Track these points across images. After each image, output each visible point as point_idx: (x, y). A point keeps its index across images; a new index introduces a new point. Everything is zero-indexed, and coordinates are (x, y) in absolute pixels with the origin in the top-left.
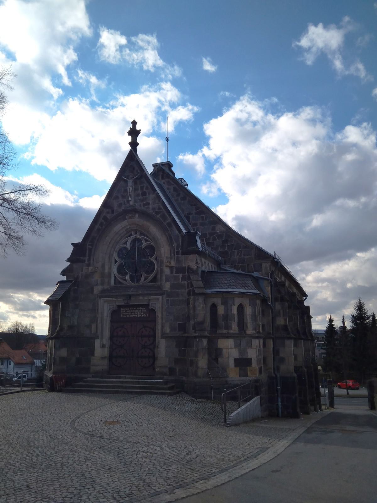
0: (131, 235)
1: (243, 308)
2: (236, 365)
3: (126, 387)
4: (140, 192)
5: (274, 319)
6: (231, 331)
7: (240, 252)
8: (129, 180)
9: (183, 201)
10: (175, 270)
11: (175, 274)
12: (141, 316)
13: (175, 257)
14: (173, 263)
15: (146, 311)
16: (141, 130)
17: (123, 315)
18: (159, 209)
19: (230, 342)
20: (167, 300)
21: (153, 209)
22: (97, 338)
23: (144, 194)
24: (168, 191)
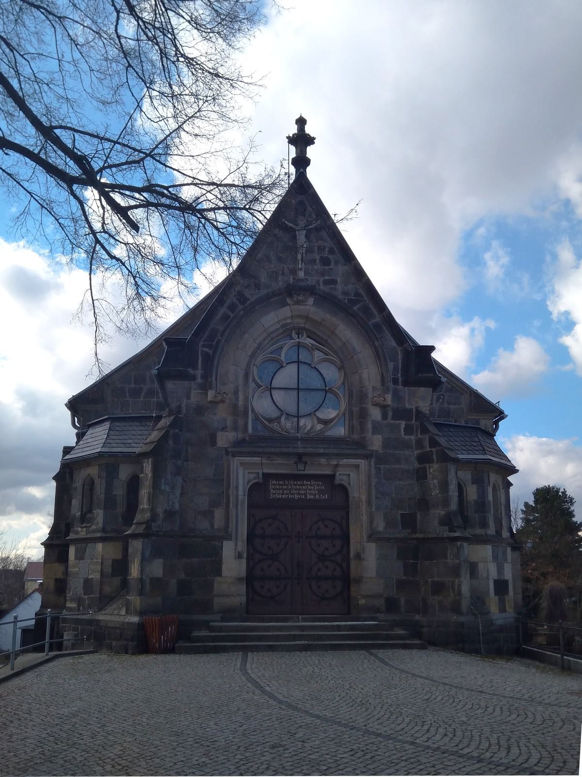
3: (320, 638)
10: (391, 414)
11: (392, 420)
12: (312, 497)
15: (323, 487)
17: (274, 494)
18: (357, 294)
19: (487, 551)
20: (378, 469)
22: (229, 538)
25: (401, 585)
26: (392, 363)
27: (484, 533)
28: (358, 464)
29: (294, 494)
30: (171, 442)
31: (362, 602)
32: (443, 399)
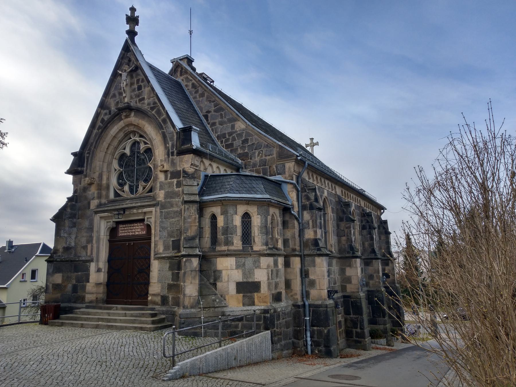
1: (250, 219)
2: (238, 292)
4: (136, 86)
5: (301, 232)
6: (232, 248)
7: (261, 152)
8: (123, 74)
9: (201, 98)
11: (170, 179)
12: (138, 233)
13: (170, 158)
14: (167, 167)
17: (121, 233)
18: (155, 103)
20: (161, 212)
21: (149, 104)
22: (92, 261)
23: (140, 88)
24: (187, 89)
25: (170, 287)
26: (171, 142)
28: (151, 210)
32: (262, 154)
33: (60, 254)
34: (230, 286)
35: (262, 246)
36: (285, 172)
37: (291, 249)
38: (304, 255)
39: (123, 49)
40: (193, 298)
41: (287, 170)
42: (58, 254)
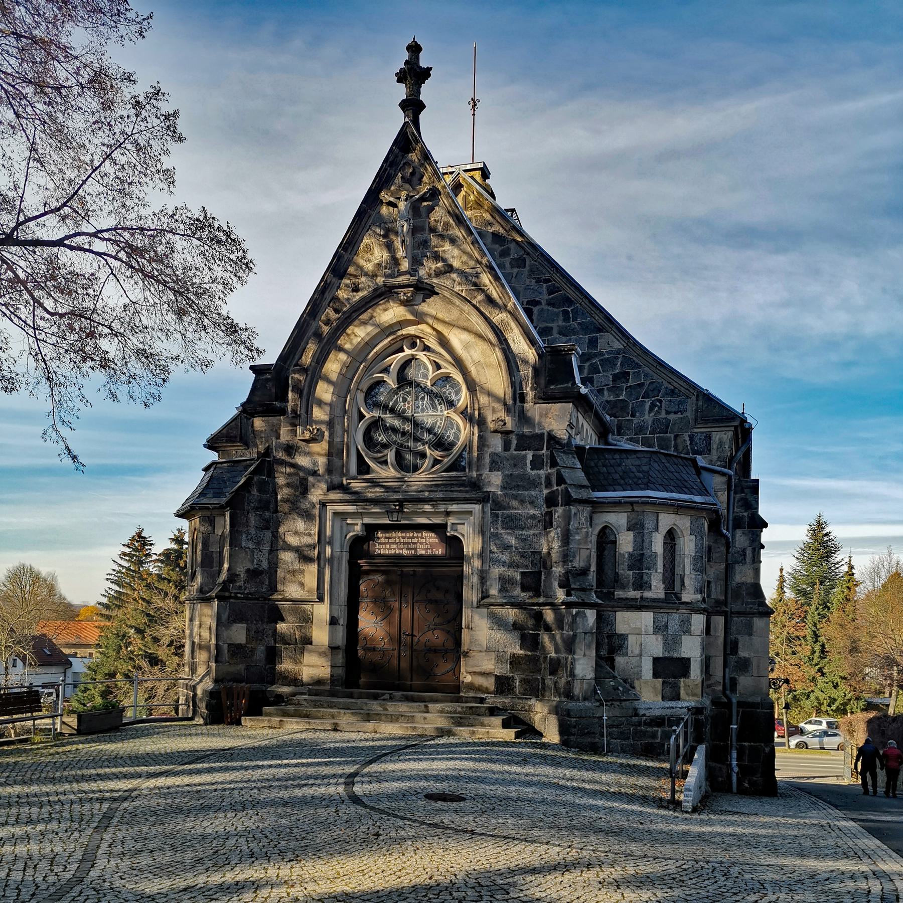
0: (402, 350)
2: (656, 675)
6: (648, 594)
7: (658, 403)
11: (515, 450)
12: (423, 552)
16: (431, 68)
19: (646, 619)
27: (638, 597)
29: (402, 549)
30: (255, 492)
31: (468, 679)
32: (660, 407)
33: (240, 583)
34: (643, 664)
35: (695, 594)
36: (710, 450)
37: (714, 601)
38: (732, 613)
39: (395, 143)
40: (587, 683)
41: (714, 446)
42: (238, 584)
